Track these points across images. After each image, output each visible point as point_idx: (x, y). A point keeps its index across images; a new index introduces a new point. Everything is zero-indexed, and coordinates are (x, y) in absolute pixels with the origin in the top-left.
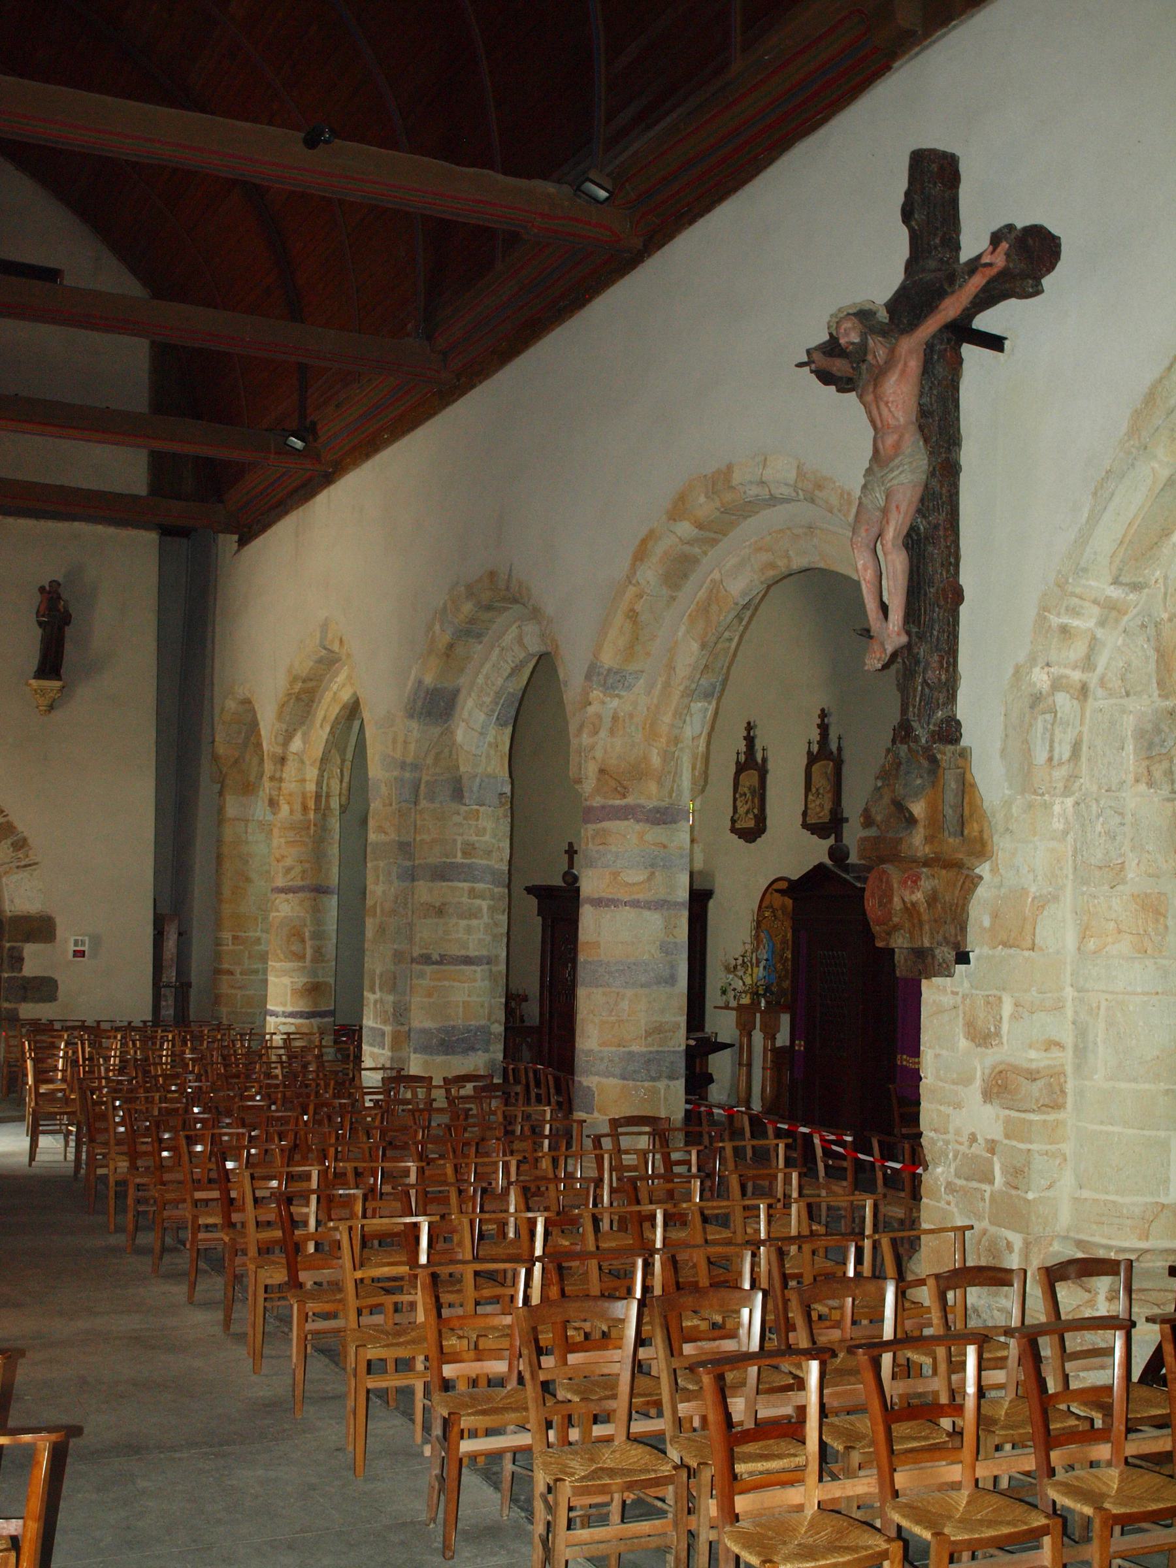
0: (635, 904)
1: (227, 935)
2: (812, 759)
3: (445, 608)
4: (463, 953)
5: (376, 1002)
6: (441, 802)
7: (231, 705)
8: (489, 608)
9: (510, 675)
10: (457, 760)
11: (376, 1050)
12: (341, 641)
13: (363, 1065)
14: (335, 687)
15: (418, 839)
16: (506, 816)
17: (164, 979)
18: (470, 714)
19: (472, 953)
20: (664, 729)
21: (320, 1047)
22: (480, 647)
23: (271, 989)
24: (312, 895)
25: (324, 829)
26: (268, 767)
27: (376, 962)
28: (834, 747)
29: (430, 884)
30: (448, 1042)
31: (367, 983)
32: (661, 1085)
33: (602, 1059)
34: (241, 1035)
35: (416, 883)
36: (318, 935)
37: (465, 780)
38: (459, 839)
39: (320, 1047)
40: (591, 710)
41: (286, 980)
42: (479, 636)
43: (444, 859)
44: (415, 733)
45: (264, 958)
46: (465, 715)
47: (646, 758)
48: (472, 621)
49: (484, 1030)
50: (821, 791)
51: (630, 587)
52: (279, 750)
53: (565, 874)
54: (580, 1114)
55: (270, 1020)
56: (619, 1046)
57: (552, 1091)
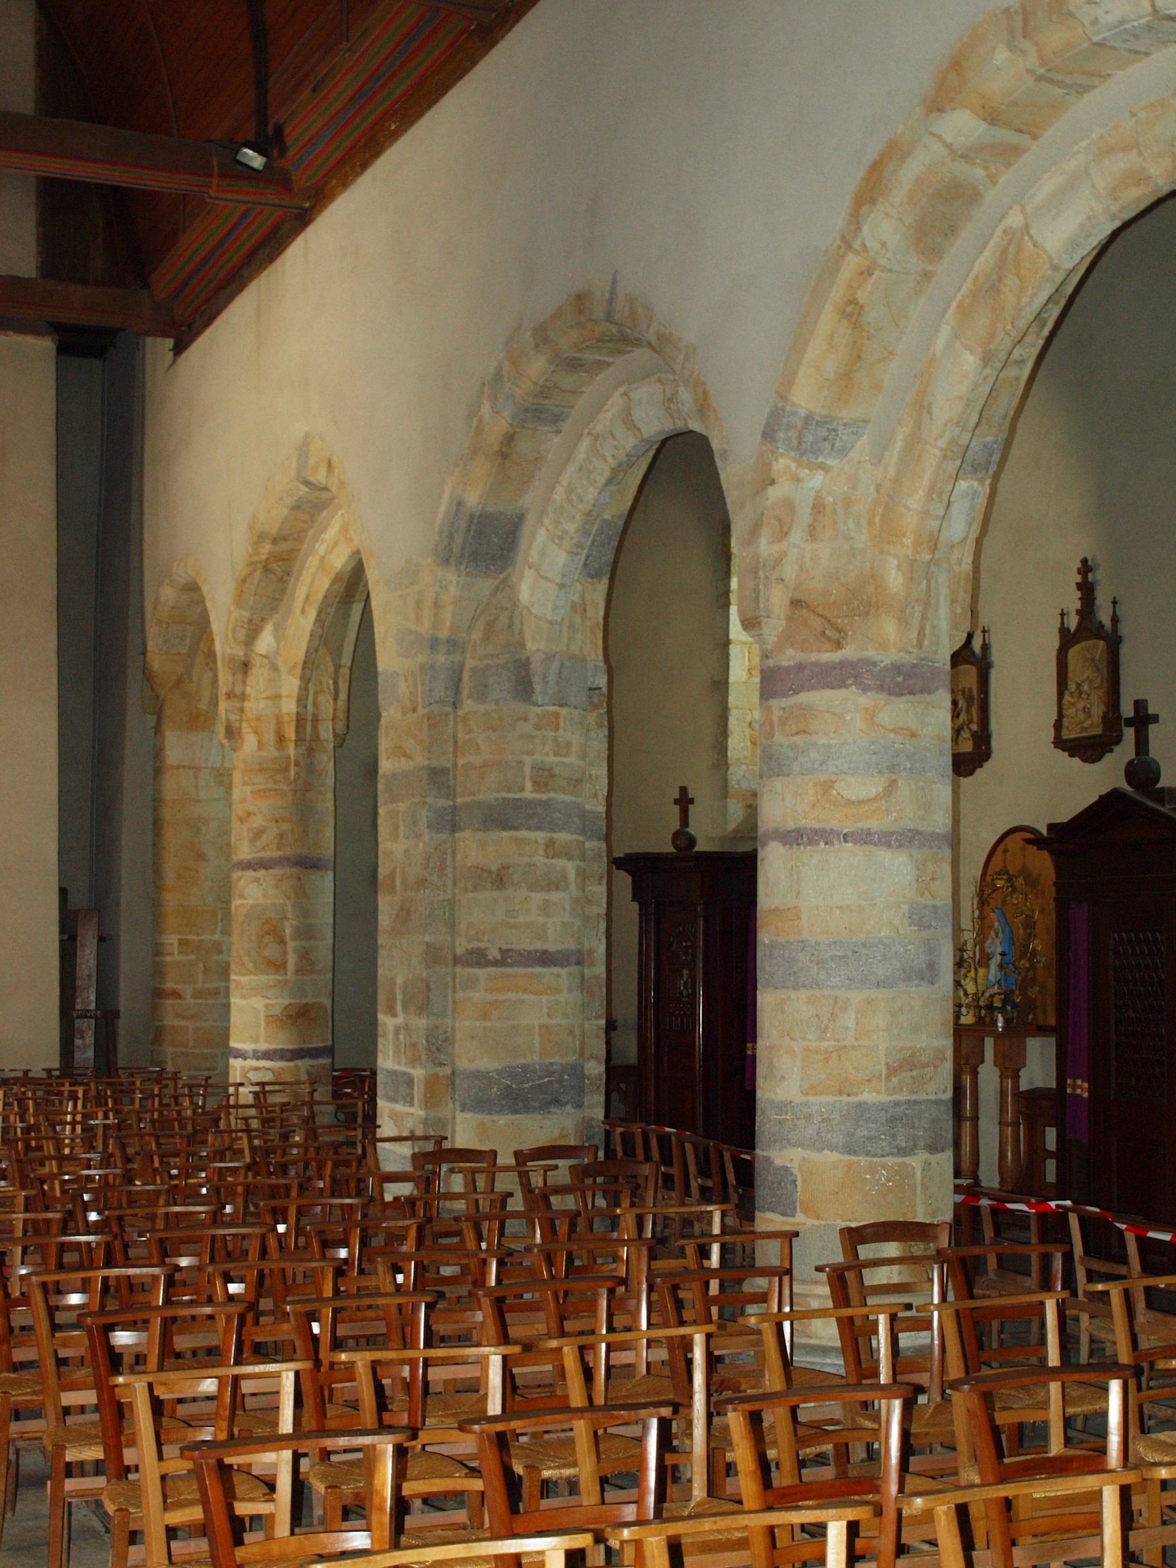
0: (864, 838)
1: (171, 940)
2: (1068, 640)
3: (498, 375)
4: (539, 946)
5: (397, 1030)
6: (497, 702)
7: (168, 594)
8: (573, 365)
9: (609, 482)
10: (521, 632)
11: (399, 1108)
12: (330, 465)
13: (380, 1133)
14: (322, 549)
15: (460, 762)
16: (601, 726)
17: (79, 1007)
18: (543, 554)
19: (552, 946)
20: (909, 521)
21: (311, 1103)
22: (557, 440)
23: (236, 1018)
24: (296, 870)
25: (311, 770)
26: (225, 678)
27: (397, 965)
28: (1104, 616)
29: (480, 835)
30: (518, 1093)
31: (382, 998)
32: (916, 1161)
33: (808, 1117)
34: (190, 1087)
35: (457, 835)
36: (306, 932)
37: (535, 665)
38: (528, 760)
39: (311, 1103)
40: (775, 493)
41: (258, 1003)
42: (556, 419)
43: (504, 795)
44: (452, 589)
45: (225, 972)
46: (534, 556)
47: (876, 578)
48: (544, 392)
49: (576, 1071)
50: (1085, 687)
51: (850, 256)
52: (239, 652)
53: (676, 836)
54: (770, 1215)
55: (236, 1063)
56: (840, 1093)
57: (692, 1169)
